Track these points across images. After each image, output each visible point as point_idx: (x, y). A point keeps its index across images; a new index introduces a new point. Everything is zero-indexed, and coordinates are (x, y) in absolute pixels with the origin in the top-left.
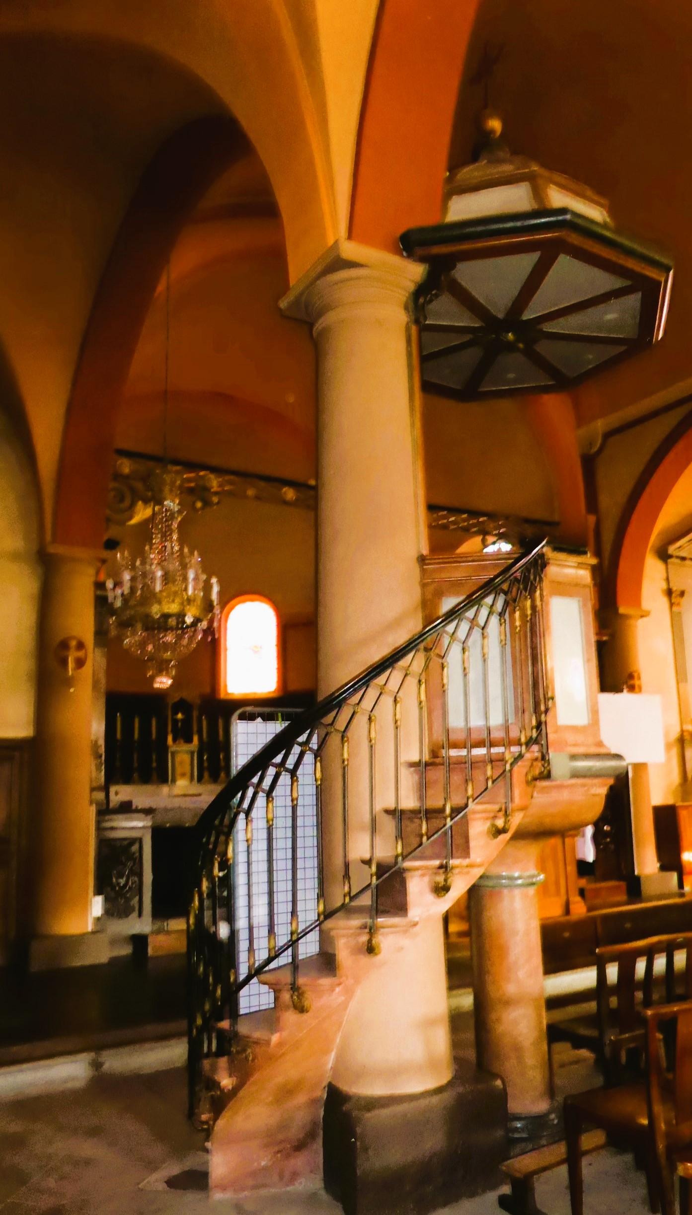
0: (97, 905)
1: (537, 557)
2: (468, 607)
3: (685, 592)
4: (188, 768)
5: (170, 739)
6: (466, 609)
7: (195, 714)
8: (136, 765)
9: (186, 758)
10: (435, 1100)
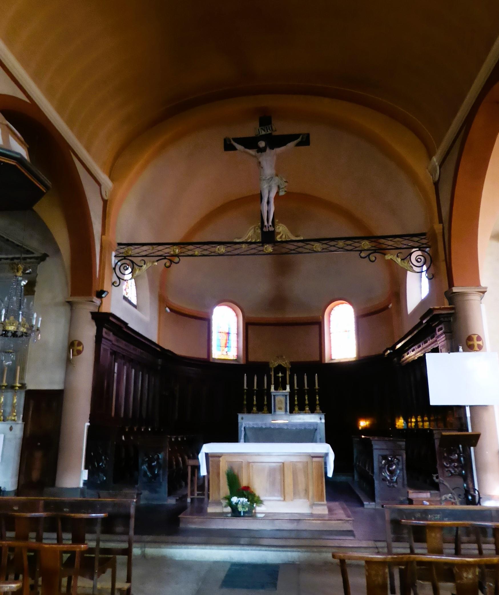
0: (85, 475)
3: (220, 583)
4: (283, 406)
5: (273, 387)
7: (288, 373)
8: (255, 403)
9: (283, 399)
10: (278, 419)
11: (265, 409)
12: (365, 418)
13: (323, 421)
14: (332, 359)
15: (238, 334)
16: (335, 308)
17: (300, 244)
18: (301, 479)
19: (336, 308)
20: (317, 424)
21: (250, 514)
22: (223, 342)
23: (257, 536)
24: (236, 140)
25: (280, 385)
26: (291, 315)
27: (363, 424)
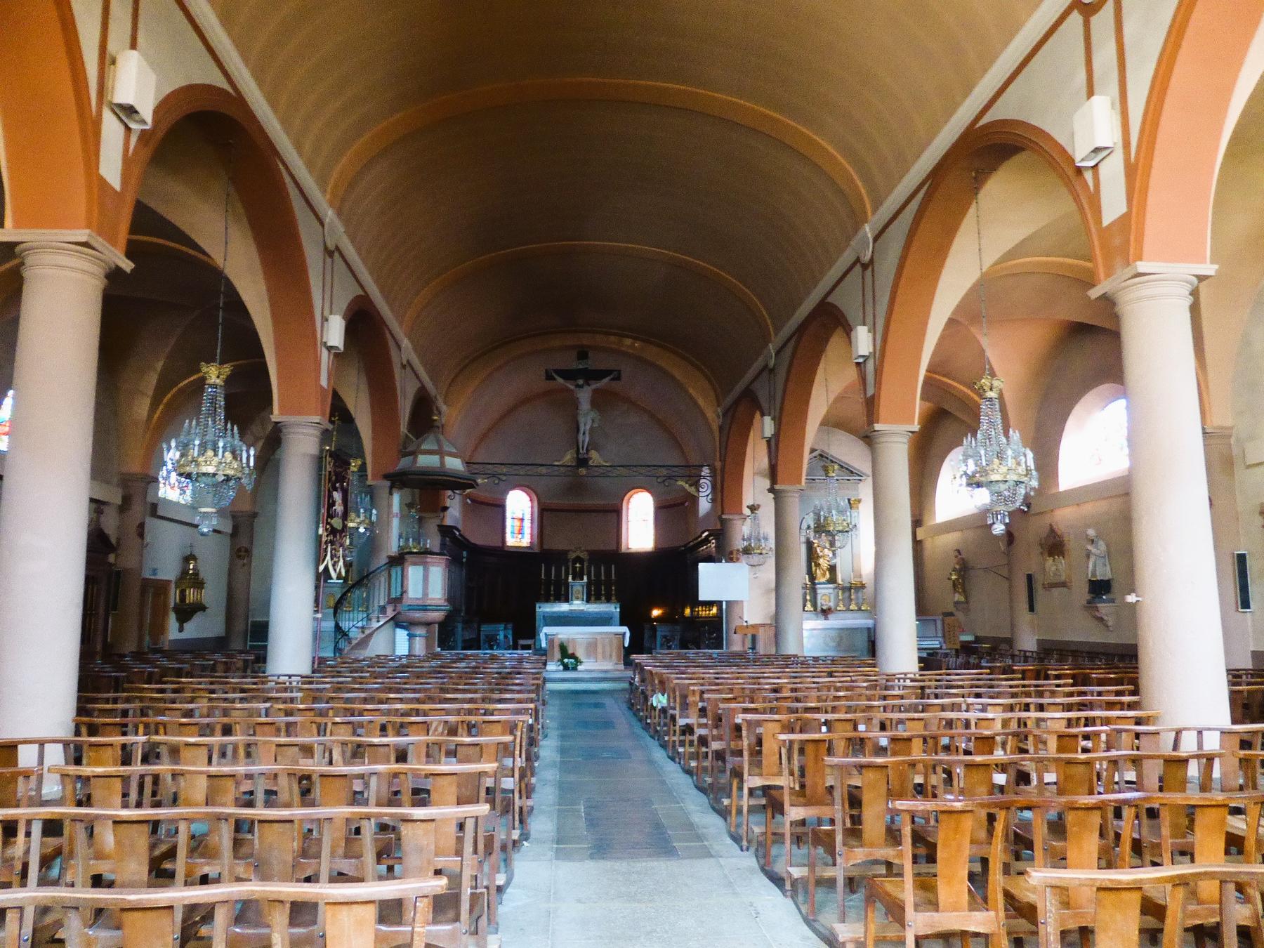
1: (1126, 683)
2: (429, 475)
4: (580, 596)
5: (570, 578)
6: (440, 475)
7: (586, 564)
9: (580, 588)
11: (563, 598)
12: (658, 606)
13: (618, 610)
14: (628, 548)
15: (532, 520)
16: (634, 496)
17: (609, 469)
18: (608, 649)
19: (635, 496)
20: (612, 612)
21: (575, 669)
22: (517, 529)
23: (983, 241)
24: (557, 372)
25: (578, 575)
26: (589, 502)
27: (656, 613)
